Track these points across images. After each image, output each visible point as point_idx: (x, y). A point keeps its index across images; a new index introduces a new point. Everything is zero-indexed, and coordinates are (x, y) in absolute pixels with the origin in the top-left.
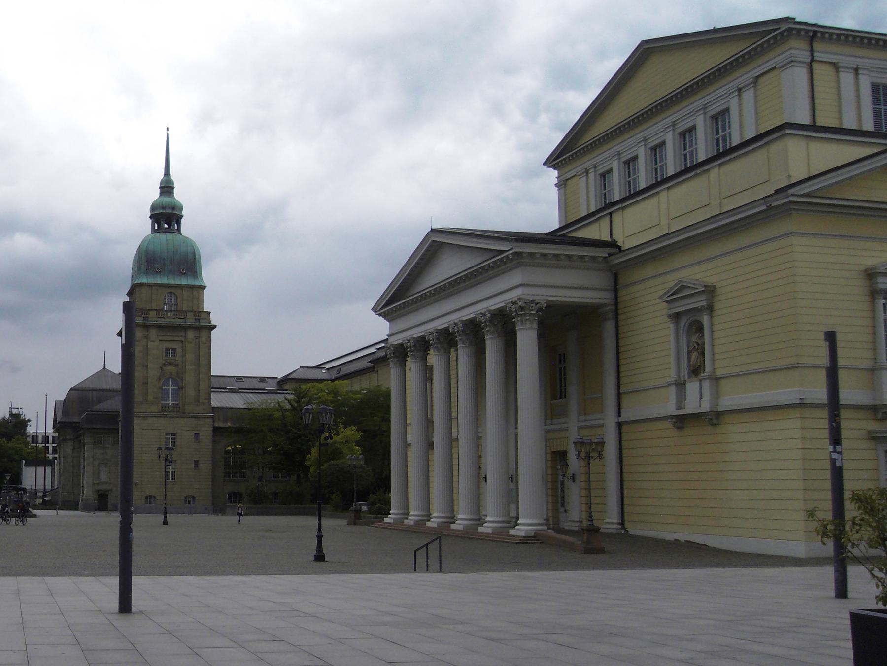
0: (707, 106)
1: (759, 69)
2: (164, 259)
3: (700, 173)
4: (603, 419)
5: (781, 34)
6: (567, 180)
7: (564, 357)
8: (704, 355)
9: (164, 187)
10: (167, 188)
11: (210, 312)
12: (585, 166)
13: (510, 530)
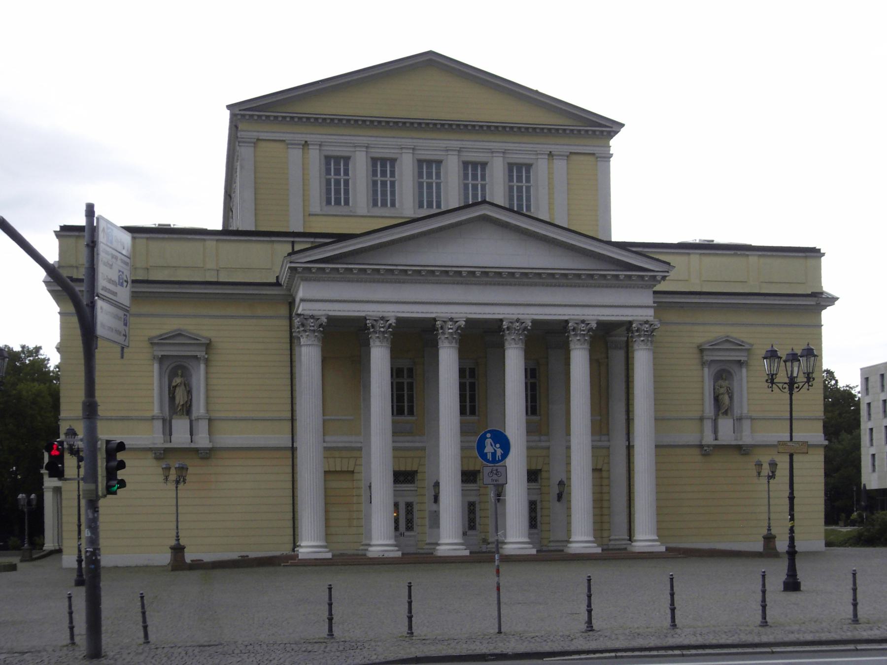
0: (506, 152)
1: (575, 148)
3: (739, 254)
6: (258, 140)
12: (309, 138)
13: (401, 556)
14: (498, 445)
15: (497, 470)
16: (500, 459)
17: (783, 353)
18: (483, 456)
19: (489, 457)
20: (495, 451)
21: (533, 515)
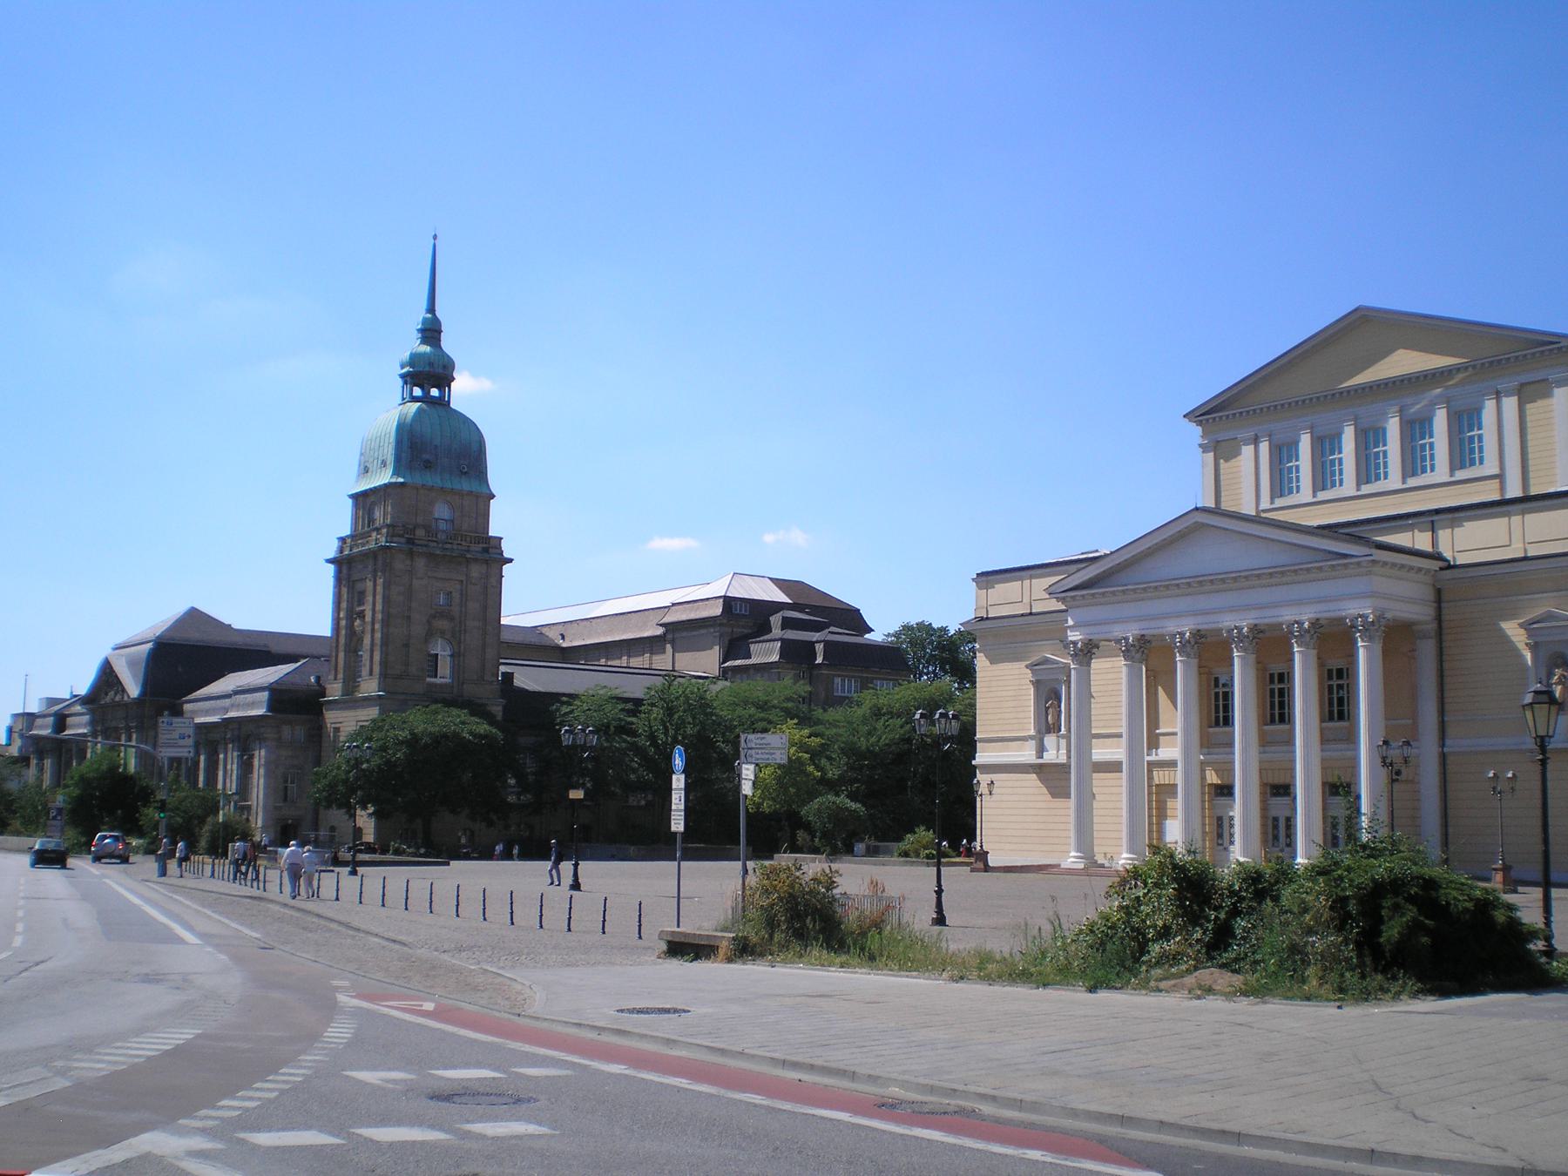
2: (436, 446)
4: (213, 875)
5: (1559, 349)
7: (1288, 676)
8: (1050, 865)
9: (429, 330)
10: (431, 332)
11: (501, 539)
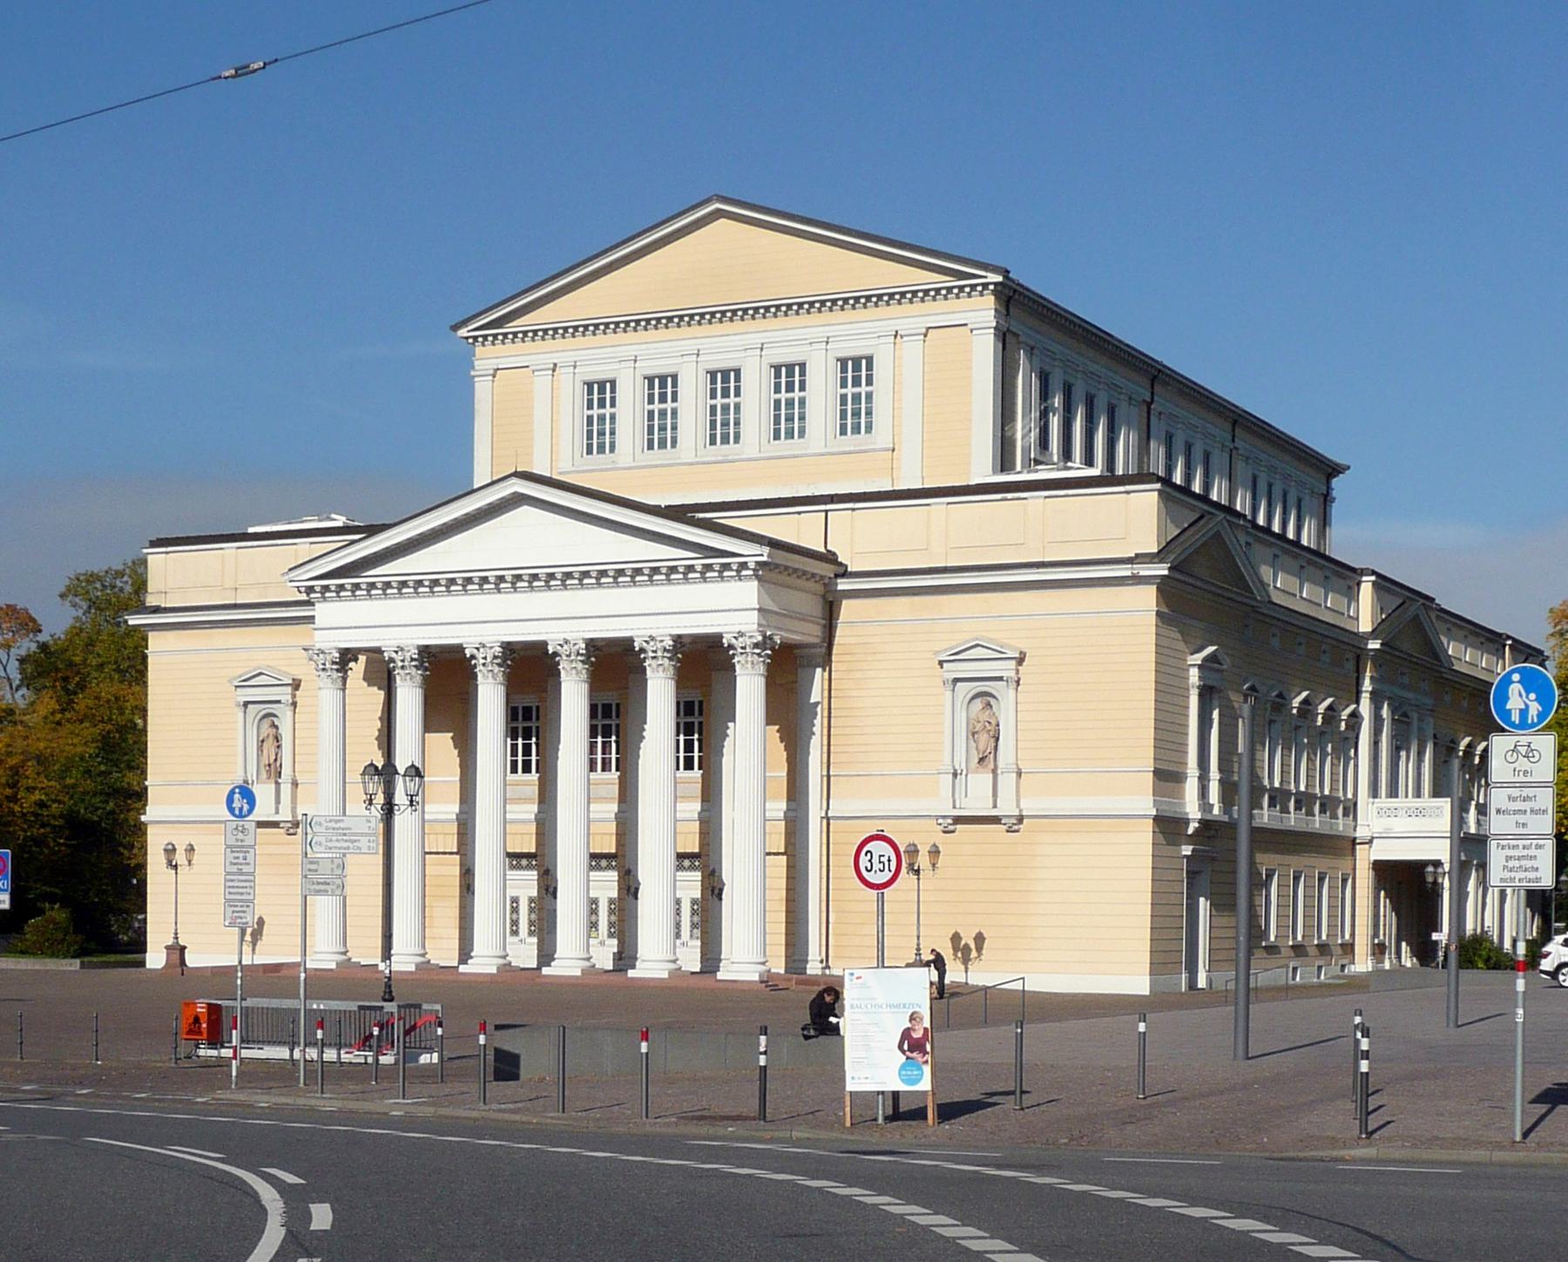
14: (1532, 696)
15: (243, 826)
16: (1535, 720)
17: (276, 744)
18: (231, 810)
19: (237, 812)
20: (1527, 706)
21: (594, 918)
